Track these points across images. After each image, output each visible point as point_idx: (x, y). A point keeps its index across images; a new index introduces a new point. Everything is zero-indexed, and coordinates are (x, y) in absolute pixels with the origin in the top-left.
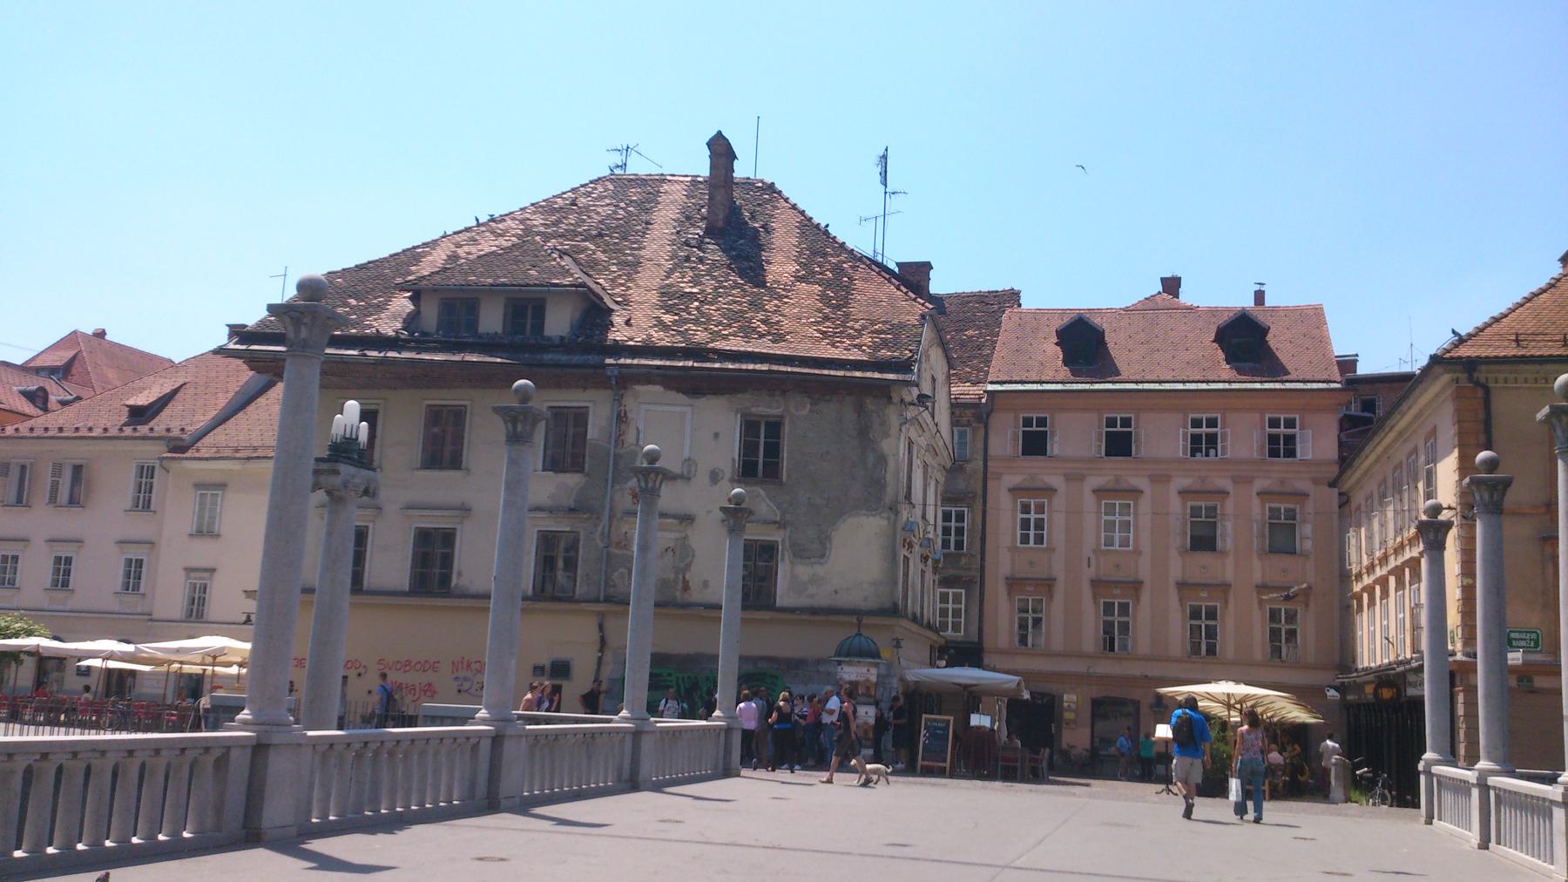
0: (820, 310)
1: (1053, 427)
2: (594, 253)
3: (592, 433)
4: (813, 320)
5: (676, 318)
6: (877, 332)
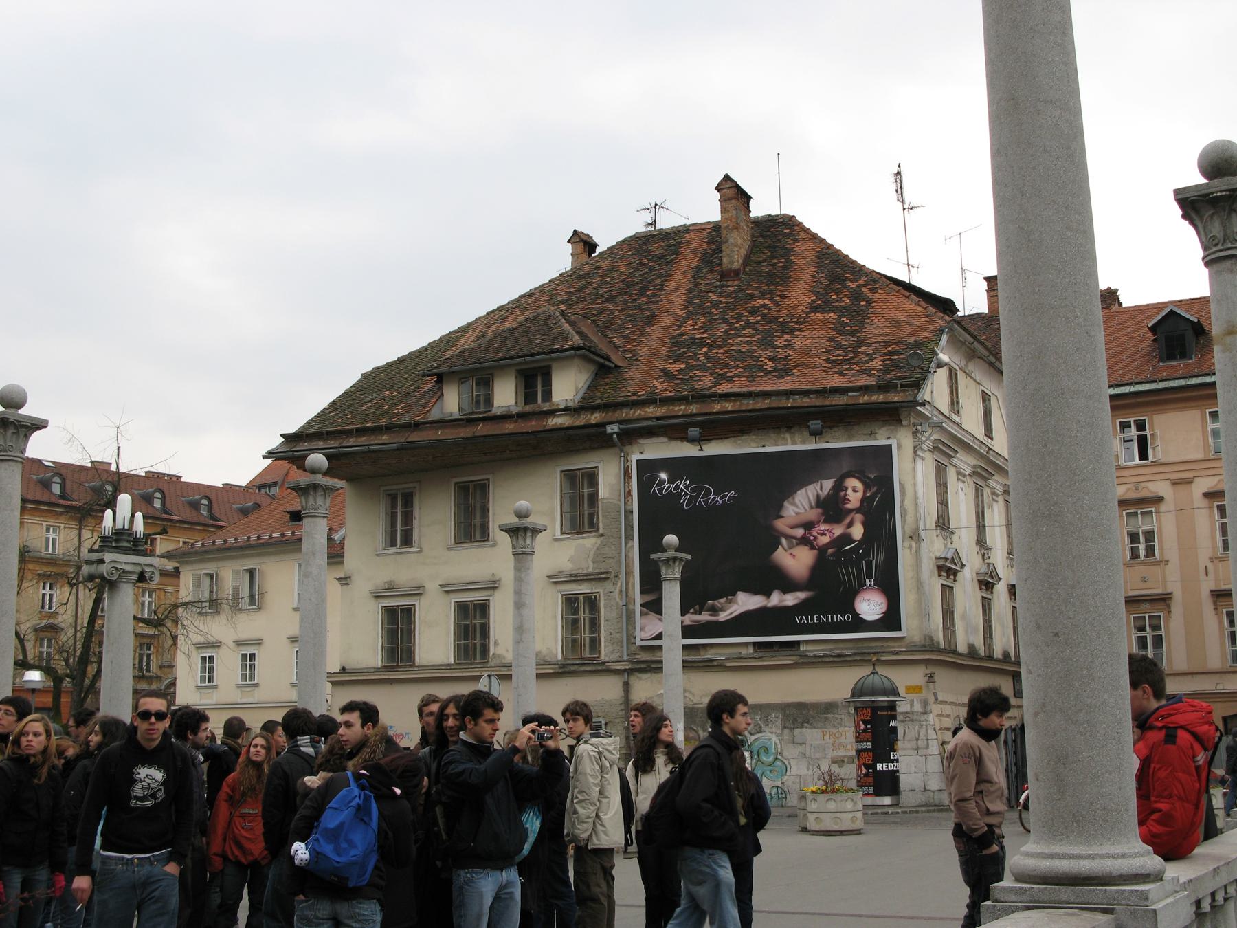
0: (832, 339)
1: (1153, 429)
2: (612, 314)
3: (604, 492)
4: (824, 350)
5: (683, 366)
6: (890, 353)
